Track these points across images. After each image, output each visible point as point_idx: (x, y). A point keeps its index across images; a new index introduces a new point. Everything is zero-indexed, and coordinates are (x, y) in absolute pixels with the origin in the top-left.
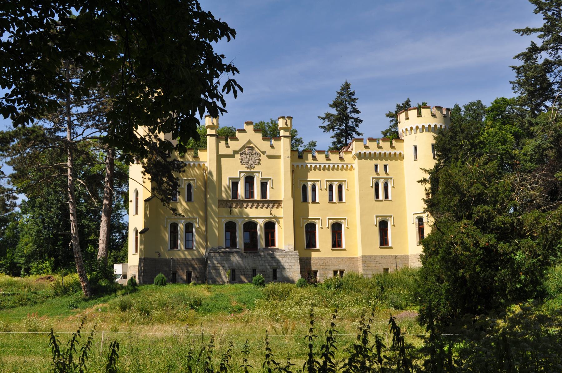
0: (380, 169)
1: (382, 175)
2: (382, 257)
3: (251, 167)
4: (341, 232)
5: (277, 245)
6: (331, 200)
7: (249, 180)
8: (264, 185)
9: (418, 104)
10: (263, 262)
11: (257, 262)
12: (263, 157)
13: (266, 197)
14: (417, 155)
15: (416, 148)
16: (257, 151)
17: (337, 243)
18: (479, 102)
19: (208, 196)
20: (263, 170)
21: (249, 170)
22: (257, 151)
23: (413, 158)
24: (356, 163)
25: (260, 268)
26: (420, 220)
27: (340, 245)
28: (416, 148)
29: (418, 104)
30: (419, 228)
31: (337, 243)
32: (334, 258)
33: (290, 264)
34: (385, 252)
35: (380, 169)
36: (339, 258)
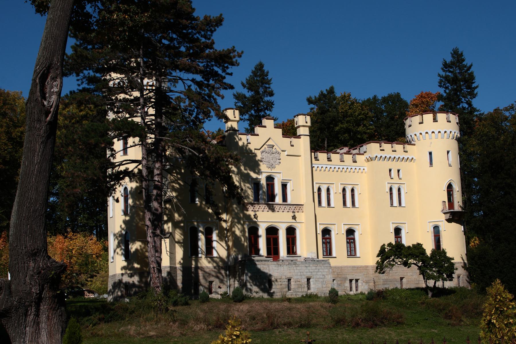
0: (394, 173)
1: (396, 180)
4: (295, 237)
5: (299, 252)
10: (298, 271)
11: (292, 271)
12: (283, 155)
13: (453, 208)
14: (429, 161)
15: (430, 153)
16: (278, 149)
17: (352, 252)
18: (398, 95)
21: (269, 170)
24: (367, 166)
25: (295, 277)
27: (330, 254)
28: (430, 153)
31: (352, 252)
32: (350, 267)
33: (323, 273)
34: (352, 262)
35: (394, 173)
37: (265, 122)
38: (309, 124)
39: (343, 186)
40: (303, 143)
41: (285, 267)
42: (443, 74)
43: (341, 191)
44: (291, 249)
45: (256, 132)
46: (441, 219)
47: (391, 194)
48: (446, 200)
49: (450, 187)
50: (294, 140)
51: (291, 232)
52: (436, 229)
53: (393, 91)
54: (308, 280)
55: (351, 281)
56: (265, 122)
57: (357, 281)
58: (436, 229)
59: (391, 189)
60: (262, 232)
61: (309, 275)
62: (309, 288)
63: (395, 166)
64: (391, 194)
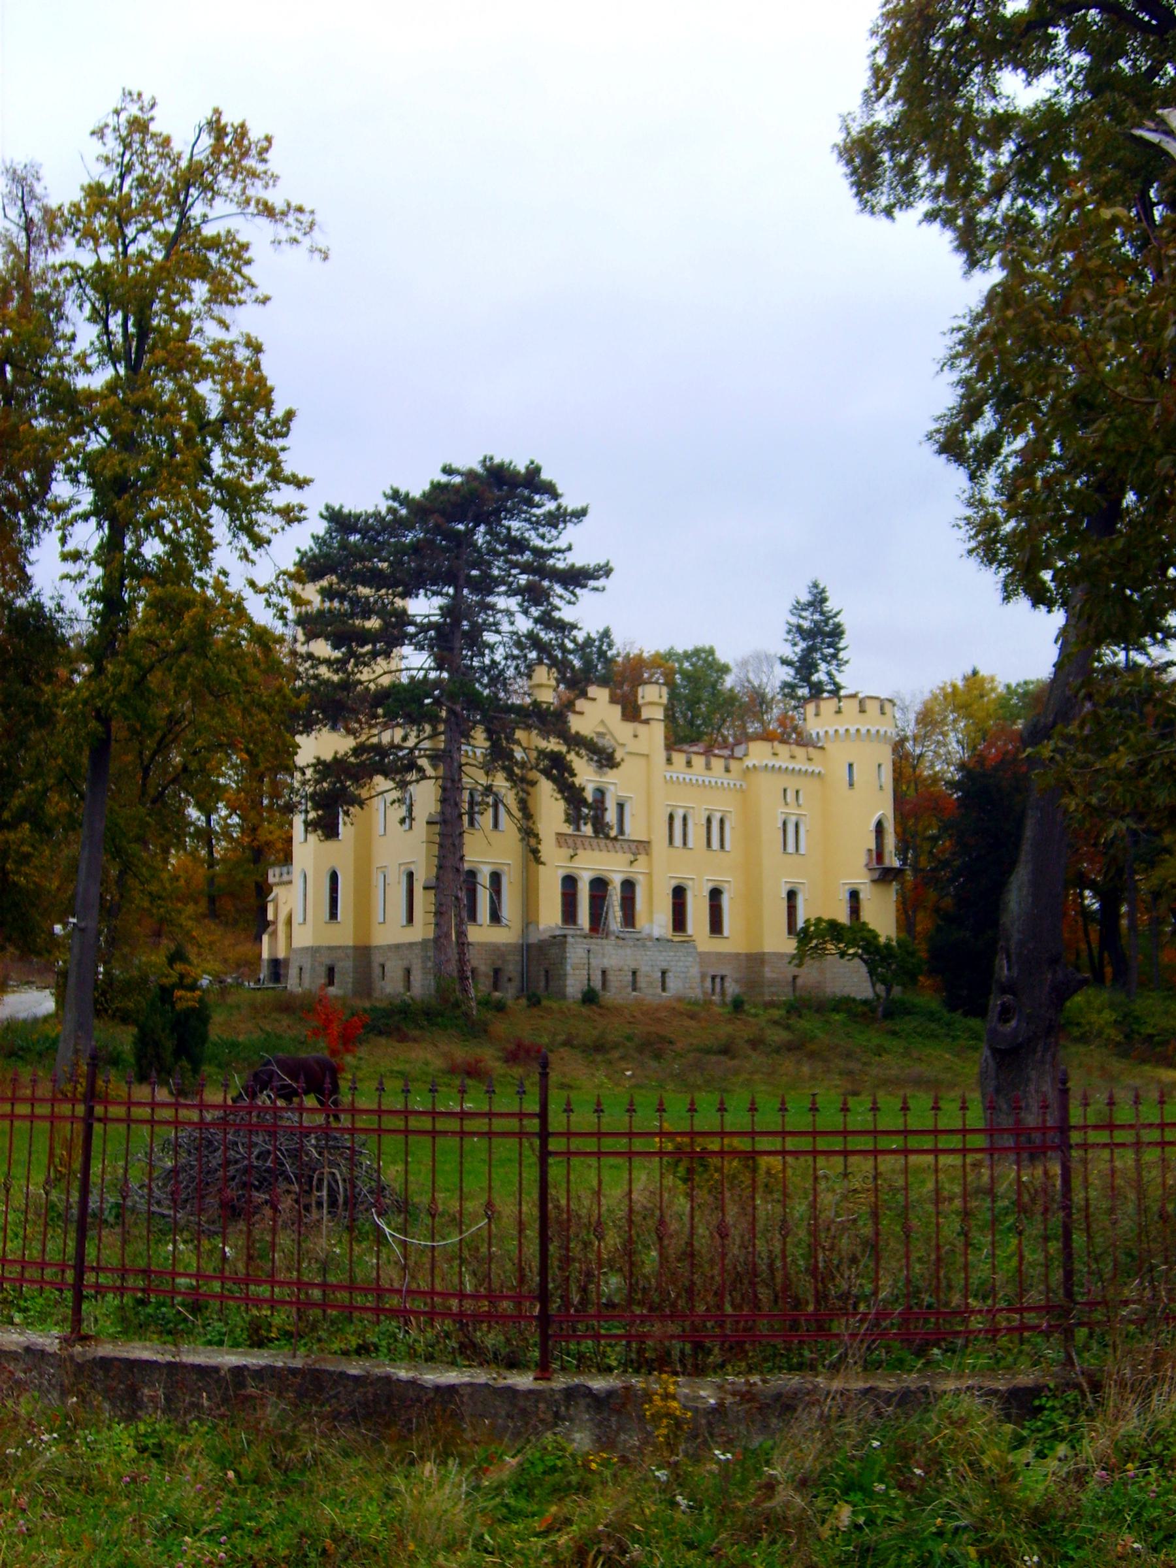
17: (716, 926)
18: (711, 652)
31: (716, 926)
37: (593, 691)
38: (665, 700)
39: (669, 810)
40: (655, 734)
41: (629, 951)
42: (794, 620)
43: (704, 821)
44: (629, 917)
45: (578, 708)
46: (861, 879)
47: (785, 831)
48: (873, 846)
49: (879, 828)
50: (642, 729)
51: (629, 886)
52: (854, 895)
53: (704, 642)
54: (664, 973)
55: (713, 978)
56: (593, 691)
57: (722, 978)
58: (854, 895)
59: (785, 824)
60: (484, 879)
61: (664, 965)
62: (664, 989)
63: (792, 784)
64: (785, 831)
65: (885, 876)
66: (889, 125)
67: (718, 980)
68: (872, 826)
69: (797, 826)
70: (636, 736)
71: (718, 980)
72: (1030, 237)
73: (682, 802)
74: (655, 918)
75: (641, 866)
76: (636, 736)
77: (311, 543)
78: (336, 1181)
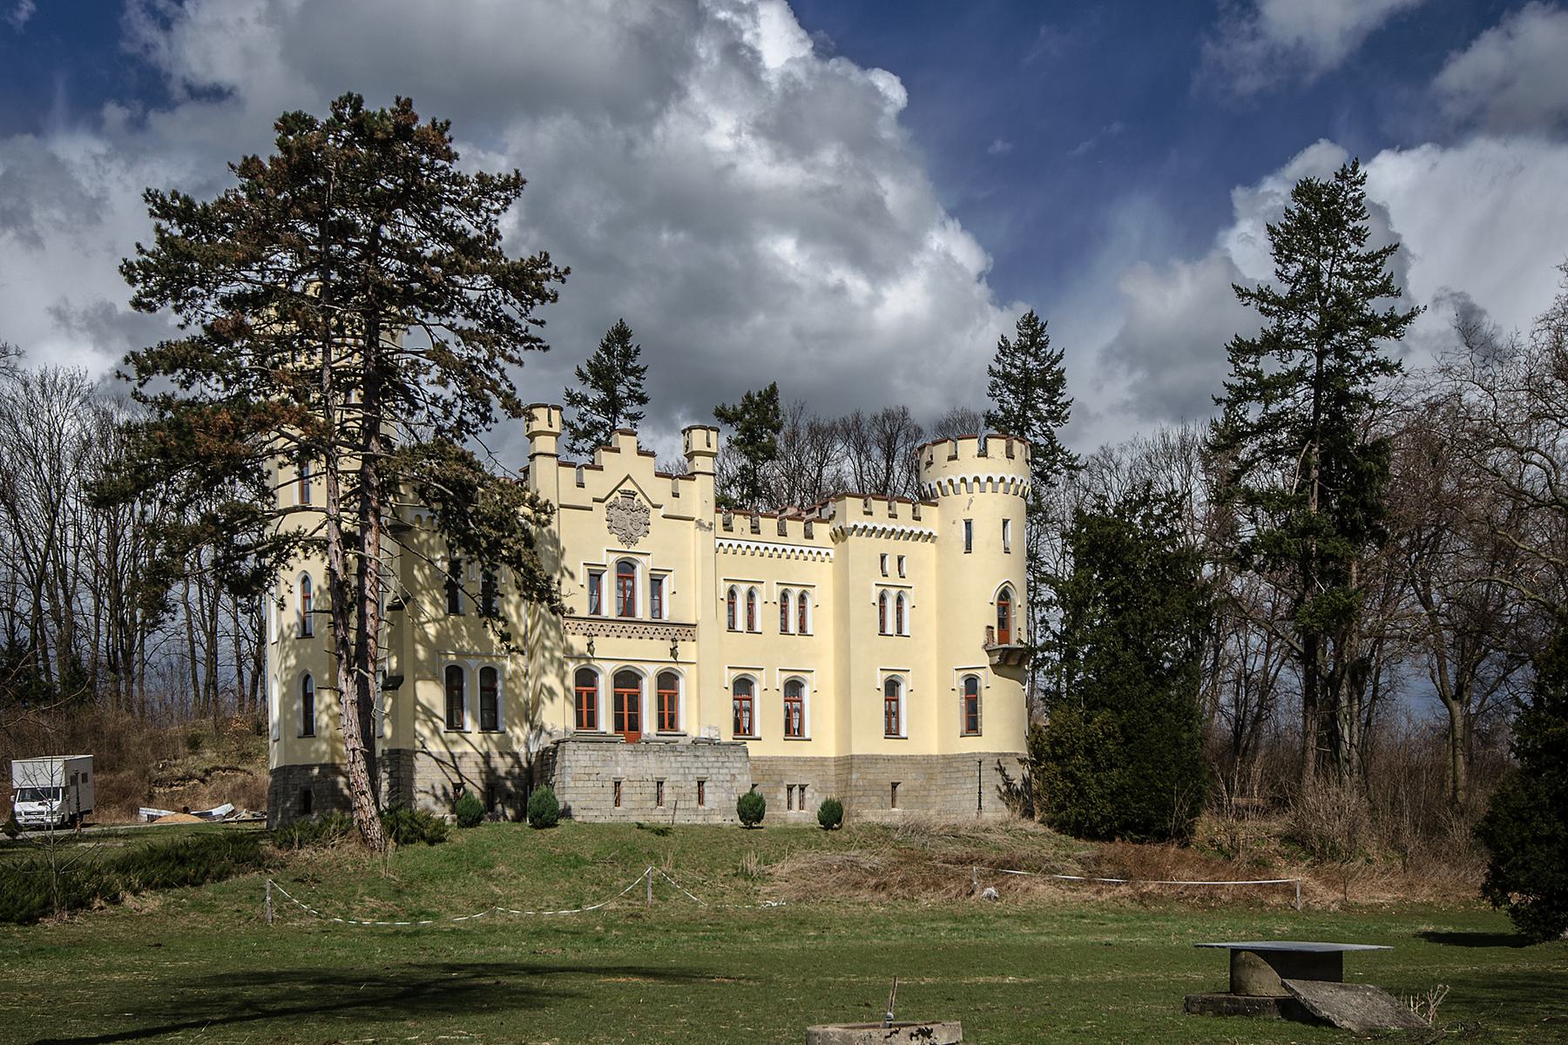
0: (891, 564)
1: (893, 578)
2: (889, 759)
3: (629, 539)
6: (784, 629)
7: (626, 569)
8: (656, 583)
9: (405, 106)
12: (655, 515)
16: (645, 502)
17: (793, 729)
19: (327, 676)
20: (652, 551)
22: (645, 502)
23: (974, 524)
26: (971, 683)
29: (405, 106)
30: (968, 718)
35: (891, 564)
36: (797, 759)
44: (668, 720)
49: (1004, 596)
55: (790, 789)
57: (802, 789)
63: (893, 547)
65: (1009, 660)
66: (810, 45)
67: (796, 790)
68: (993, 595)
69: (900, 600)
70: (676, 495)
71: (796, 790)
72: (1117, 676)
73: (743, 568)
74: (703, 711)
75: (687, 650)
76: (676, 495)
77: (389, 106)
78: (225, 998)
